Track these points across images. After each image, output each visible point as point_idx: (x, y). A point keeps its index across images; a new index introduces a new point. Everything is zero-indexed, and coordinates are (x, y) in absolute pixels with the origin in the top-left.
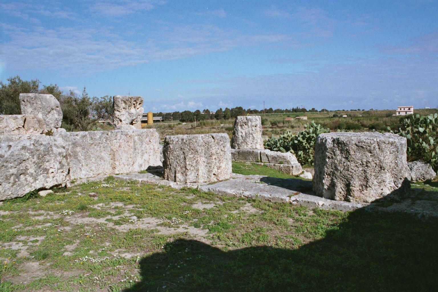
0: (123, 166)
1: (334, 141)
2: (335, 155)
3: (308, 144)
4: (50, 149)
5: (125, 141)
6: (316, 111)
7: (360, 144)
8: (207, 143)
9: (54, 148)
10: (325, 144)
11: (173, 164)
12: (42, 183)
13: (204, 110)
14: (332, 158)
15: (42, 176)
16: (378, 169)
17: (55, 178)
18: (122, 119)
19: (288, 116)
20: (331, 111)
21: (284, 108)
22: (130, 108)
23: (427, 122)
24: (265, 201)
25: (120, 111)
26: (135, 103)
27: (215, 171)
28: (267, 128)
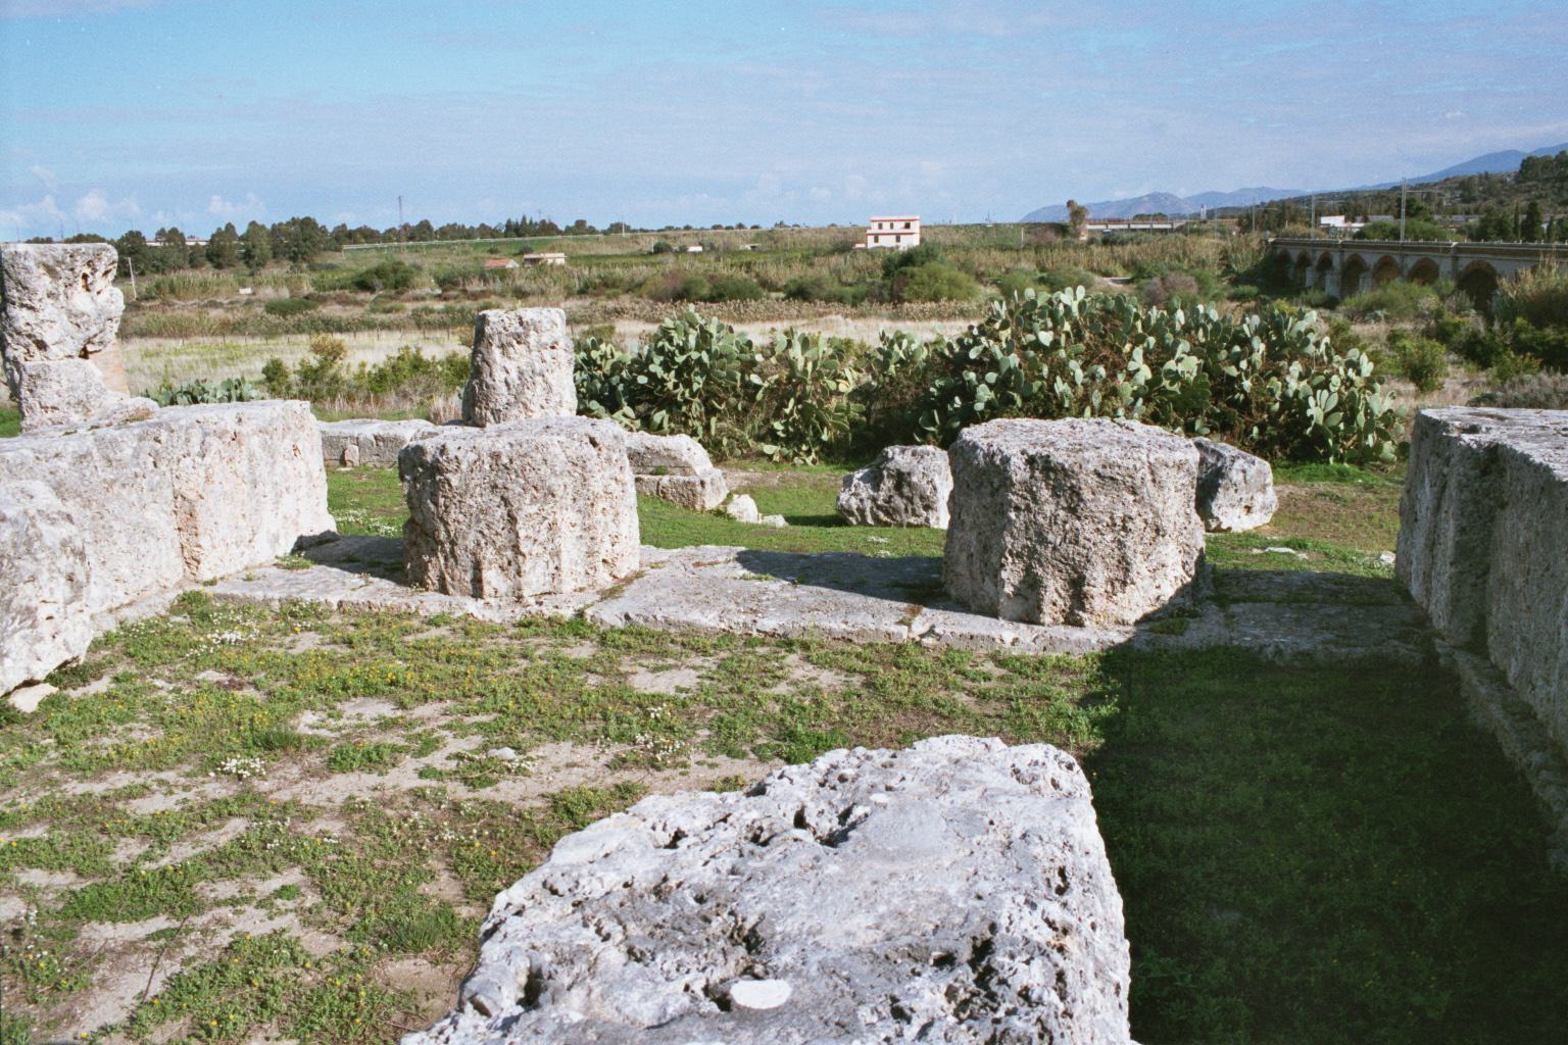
0: (223, 548)
1: (1031, 461)
2: (1035, 500)
3: (686, 387)
4: (31, 531)
5: (222, 458)
6: (592, 231)
7: (1108, 472)
8: (580, 463)
9: (43, 526)
10: (1006, 470)
11: (464, 538)
12: (22, 664)
13: (161, 233)
15: (17, 637)
16: (1149, 534)
17: (59, 639)
18: (48, 339)
19: (492, 251)
21: (470, 221)
22: (69, 292)
23: (1057, 311)
24: (833, 643)
25: (37, 305)
26: (87, 271)
27: (605, 550)
28: (423, 299)
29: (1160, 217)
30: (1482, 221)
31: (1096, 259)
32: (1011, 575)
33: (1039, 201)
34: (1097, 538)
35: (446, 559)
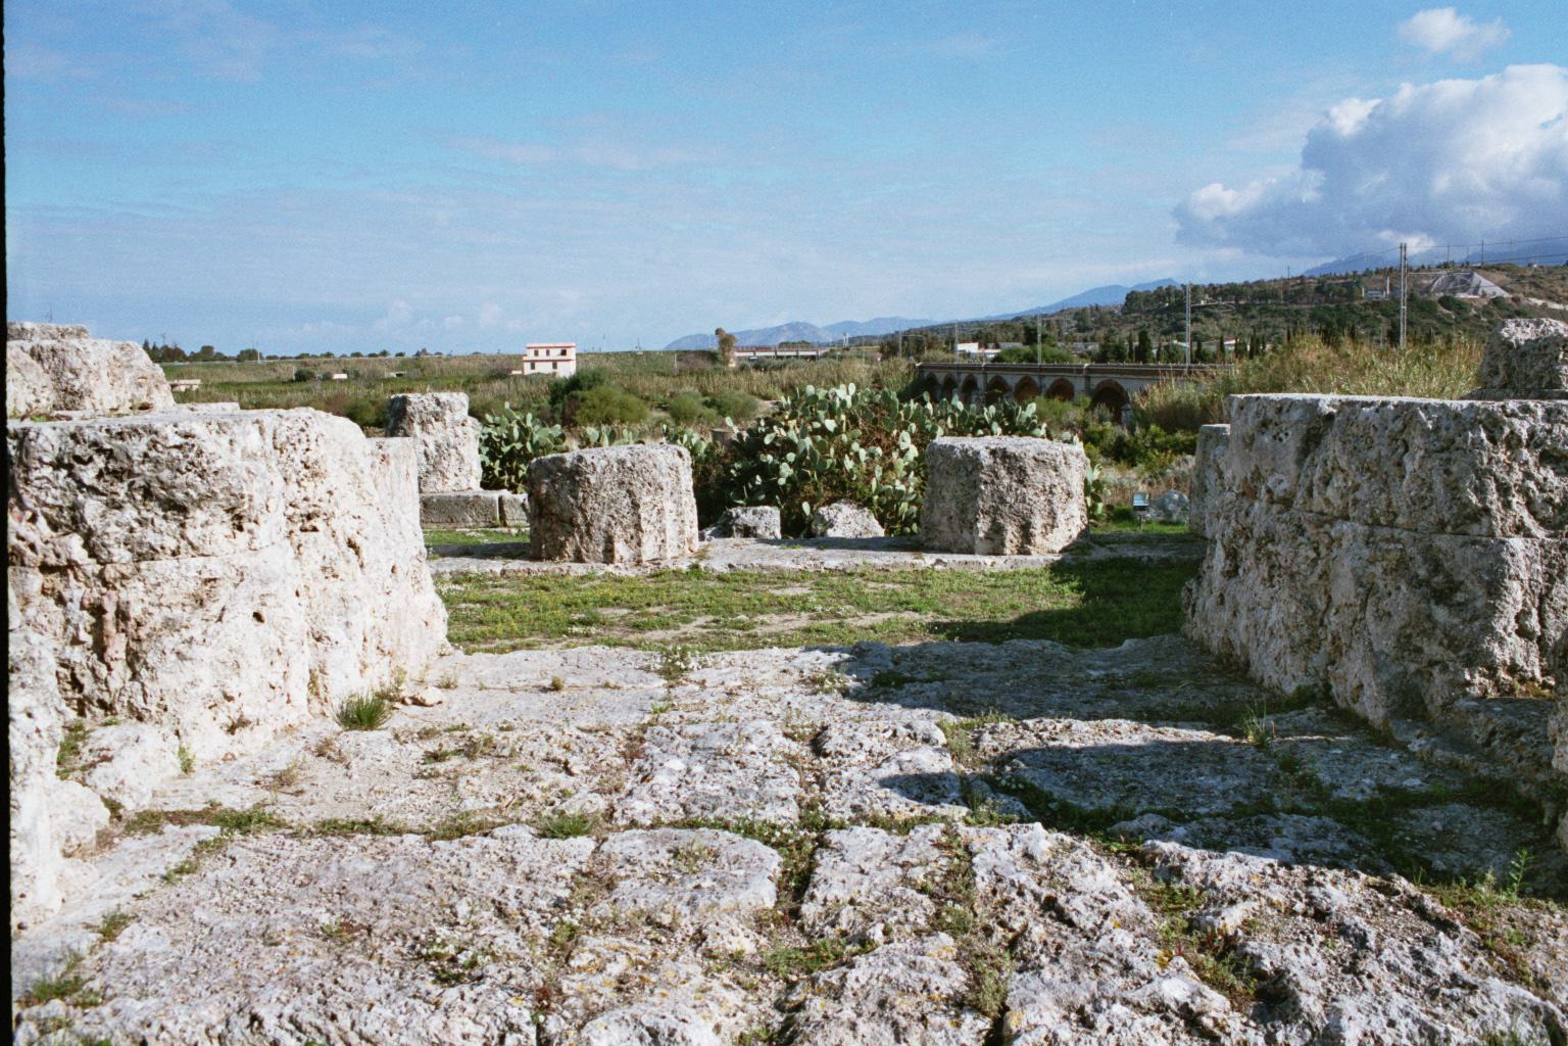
1: (993, 453)
2: (997, 477)
7: (1040, 457)
14: (993, 482)
16: (1065, 497)
20: (283, 358)
29: (805, 345)
30: (1102, 346)
31: (756, 383)
32: (983, 525)
33: (694, 328)
34: (1035, 498)
35: (581, 538)
